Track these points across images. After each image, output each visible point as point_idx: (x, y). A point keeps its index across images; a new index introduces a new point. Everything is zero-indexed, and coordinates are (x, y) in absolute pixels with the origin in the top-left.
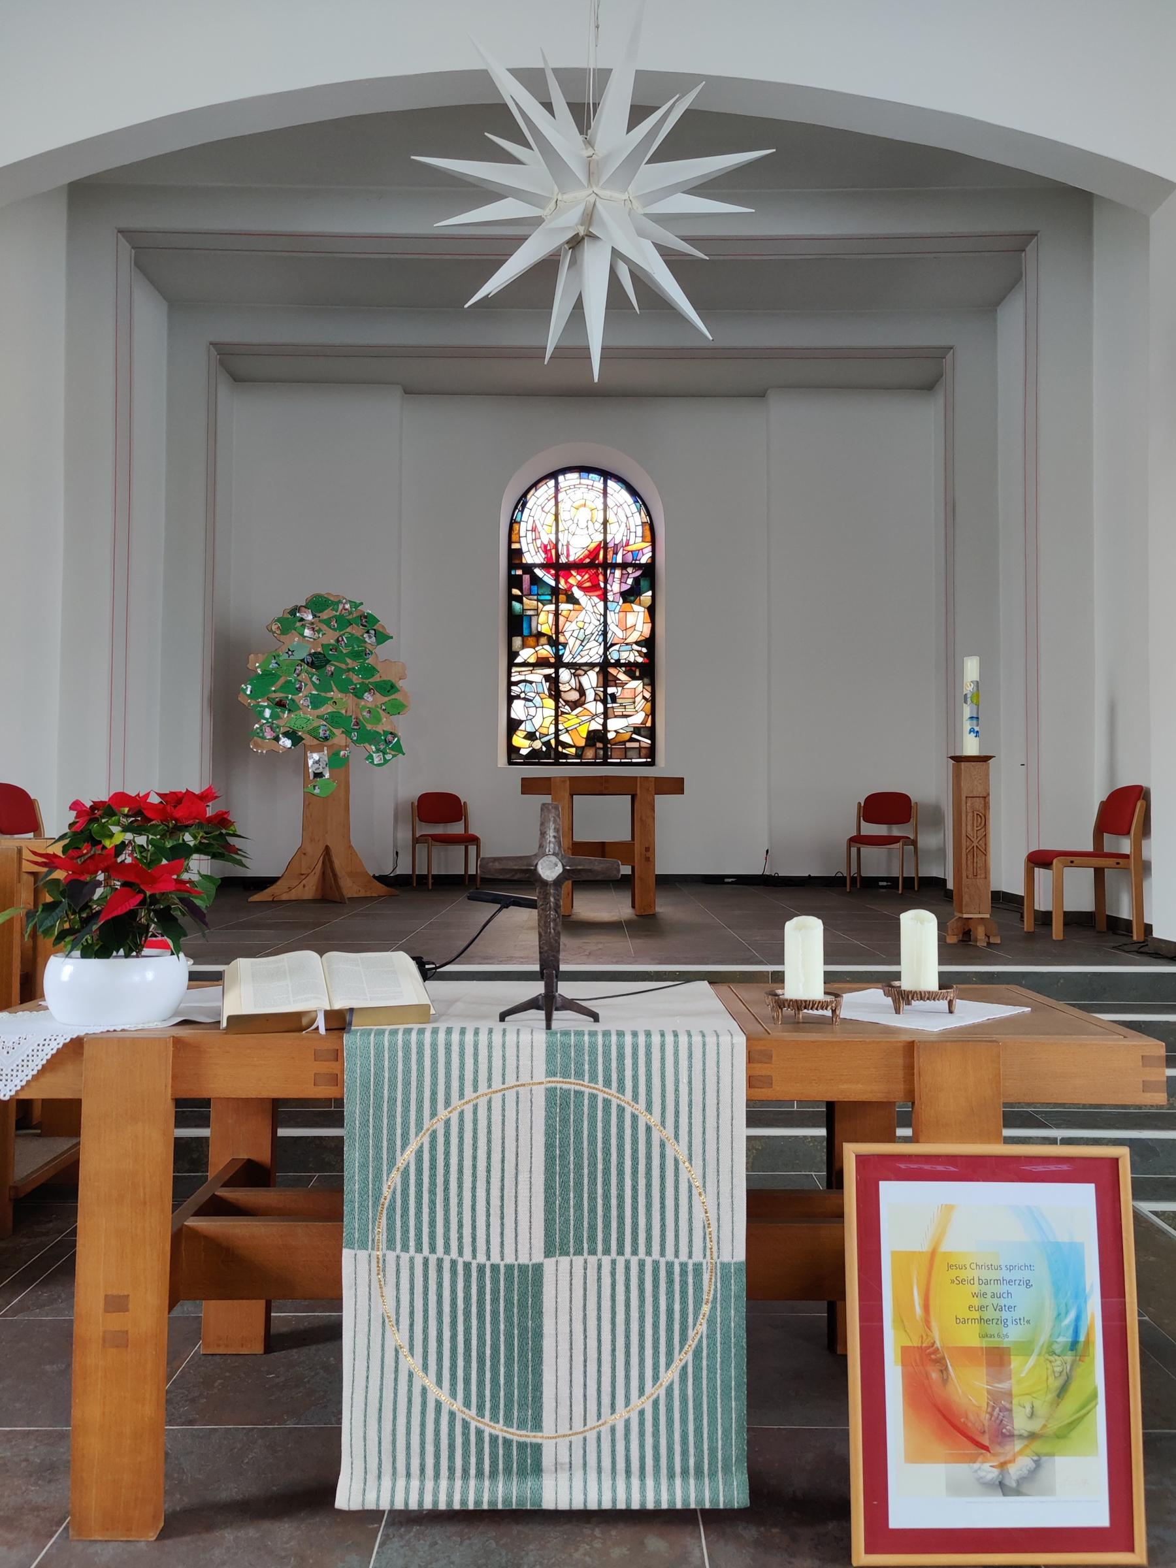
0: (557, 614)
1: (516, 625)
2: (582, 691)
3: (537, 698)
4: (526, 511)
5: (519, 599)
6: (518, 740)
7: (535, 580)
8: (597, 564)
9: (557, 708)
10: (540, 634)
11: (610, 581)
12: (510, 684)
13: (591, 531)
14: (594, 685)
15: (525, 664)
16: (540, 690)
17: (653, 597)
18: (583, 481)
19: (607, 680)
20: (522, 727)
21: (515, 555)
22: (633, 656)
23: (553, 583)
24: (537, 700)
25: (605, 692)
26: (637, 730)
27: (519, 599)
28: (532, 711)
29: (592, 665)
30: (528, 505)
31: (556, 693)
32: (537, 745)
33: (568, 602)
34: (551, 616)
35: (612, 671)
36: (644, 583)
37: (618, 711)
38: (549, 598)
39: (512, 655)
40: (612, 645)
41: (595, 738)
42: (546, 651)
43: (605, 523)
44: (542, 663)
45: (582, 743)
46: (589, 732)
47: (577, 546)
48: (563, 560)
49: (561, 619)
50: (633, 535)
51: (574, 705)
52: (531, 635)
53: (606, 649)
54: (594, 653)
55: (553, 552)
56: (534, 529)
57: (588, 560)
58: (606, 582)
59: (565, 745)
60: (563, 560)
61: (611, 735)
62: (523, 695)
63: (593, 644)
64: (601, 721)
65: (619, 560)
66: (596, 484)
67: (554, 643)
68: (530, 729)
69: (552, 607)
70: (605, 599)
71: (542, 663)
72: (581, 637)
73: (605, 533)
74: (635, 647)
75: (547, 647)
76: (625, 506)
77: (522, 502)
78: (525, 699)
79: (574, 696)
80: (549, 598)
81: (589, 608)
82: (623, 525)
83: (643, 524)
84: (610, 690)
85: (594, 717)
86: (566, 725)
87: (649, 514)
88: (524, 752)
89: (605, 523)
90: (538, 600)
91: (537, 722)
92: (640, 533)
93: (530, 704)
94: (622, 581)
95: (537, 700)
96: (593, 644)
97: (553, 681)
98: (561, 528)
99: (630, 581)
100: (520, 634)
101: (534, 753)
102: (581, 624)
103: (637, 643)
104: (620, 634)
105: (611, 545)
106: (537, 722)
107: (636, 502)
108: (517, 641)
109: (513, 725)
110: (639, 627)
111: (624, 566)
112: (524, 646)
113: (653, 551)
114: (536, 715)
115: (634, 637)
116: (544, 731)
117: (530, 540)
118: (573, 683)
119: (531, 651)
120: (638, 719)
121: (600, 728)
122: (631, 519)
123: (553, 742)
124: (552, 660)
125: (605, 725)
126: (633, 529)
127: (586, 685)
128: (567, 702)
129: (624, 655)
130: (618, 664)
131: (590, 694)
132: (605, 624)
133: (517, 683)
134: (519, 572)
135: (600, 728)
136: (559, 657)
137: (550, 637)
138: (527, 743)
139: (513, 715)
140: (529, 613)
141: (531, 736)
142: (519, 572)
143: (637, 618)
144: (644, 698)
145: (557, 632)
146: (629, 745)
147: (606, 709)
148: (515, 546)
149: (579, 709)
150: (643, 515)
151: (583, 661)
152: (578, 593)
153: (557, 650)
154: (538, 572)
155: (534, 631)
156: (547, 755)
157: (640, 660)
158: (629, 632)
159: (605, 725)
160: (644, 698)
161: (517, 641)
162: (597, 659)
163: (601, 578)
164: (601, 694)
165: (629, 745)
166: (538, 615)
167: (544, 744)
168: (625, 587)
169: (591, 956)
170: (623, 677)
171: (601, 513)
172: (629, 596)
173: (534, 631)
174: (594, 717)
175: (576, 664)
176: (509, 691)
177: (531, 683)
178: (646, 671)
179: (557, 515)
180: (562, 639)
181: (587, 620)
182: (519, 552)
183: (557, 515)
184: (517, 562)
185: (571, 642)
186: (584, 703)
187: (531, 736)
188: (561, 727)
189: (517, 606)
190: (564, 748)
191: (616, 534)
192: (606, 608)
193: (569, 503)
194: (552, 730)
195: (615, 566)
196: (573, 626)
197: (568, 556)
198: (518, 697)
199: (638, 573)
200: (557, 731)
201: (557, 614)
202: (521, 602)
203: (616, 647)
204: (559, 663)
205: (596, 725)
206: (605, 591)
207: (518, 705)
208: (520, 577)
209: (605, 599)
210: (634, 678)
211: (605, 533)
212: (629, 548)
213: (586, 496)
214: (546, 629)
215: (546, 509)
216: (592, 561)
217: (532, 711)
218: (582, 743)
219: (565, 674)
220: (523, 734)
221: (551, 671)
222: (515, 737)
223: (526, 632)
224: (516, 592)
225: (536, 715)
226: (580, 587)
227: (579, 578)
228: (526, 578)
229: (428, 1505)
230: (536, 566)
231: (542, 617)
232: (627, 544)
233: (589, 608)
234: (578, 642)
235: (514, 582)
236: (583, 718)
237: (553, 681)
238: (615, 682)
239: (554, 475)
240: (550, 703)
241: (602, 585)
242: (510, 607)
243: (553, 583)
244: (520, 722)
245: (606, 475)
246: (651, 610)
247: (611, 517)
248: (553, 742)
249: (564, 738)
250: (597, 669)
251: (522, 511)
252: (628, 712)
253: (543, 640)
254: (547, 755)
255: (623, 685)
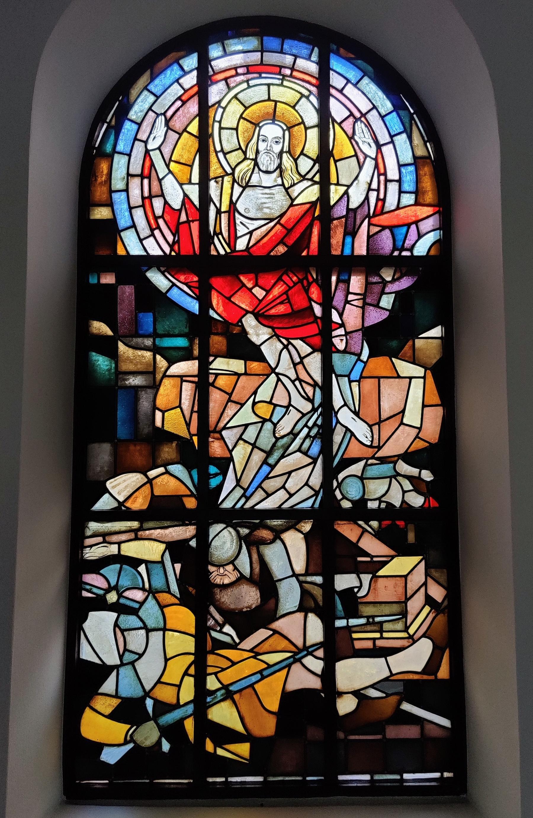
0: (203, 384)
1: (101, 422)
2: (265, 582)
3: (151, 603)
4: (128, 128)
5: (108, 346)
6: (98, 726)
7: (153, 300)
8: (308, 255)
9: (201, 633)
10: (164, 436)
11: (338, 299)
12: (78, 566)
13: (290, 177)
14: (300, 566)
15: (120, 513)
16: (158, 582)
17: (448, 342)
18: (271, 58)
19: (330, 553)
20: (109, 686)
21: (95, 239)
22: (399, 492)
23: (194, 306)
24: (150, 612)
25: (328, 586)
26: (412, 688)
27: (108, 346)
28: (136, 640)
29: (292, 517)
30: (135, 113)
31: (197, 589)
32: (148, 734)
33: (230, 354)
34: (188, 389)
35: (348, 531)
36: (422, 309)
37: (363, 639)
38: (181, 342)
39: (85, 490)
40: (347, 462)
41: (307, 710)
42: (174, 479)
43: (325, 157)
44: (162, 510)
45: (267, 727)
46: (288, 697)
47: (256, 209)
48: (220, 248)
49: (216, 398)
50: (393, 188)
51: (247, 622)
52: (136, 437)
53: (330, 473)
54: (298, 482)
55: (195, 227)
56: (147, 172)
57: (281, 249)
58: (327, 304)
59: (225, 735)
60: (220, 248)
61: (346, 705)
62: (112, 597)
63: (296, 459)
64: (317, 666)
65: (361, 248)
66: (301, 63)
67: (199, 454)
68: (129, 689)
69: (188, 367)
70: (326, 350)
71: (162, 510)
72: (266, 441)
73: (325, 184)
74: (403, 467)
75: (177, 469)
76: (373, 117)
77: (114, 105)
78: (120, 609)
79: (250, 597)
80: (181, 342)
81: (285, 367)
82: (369, 165)
83: (417, 161)
84: (343, 582)
85: (299, 653)
86: (227, 677)
87: (432, 135)
88: (111, 756)
89: (325, 157)
90: (156, 350)
91: (149, 669)
92: (409, 185)
93: (130, 621)
94: (368, 300)
95: (150, 612)
96: (296, 459)
97: (193, 560)
98: (214, 170)
99: (387, 301)
100: (108, 434)
101: (139, 758)
102: (264, 410)
103: (408, 457)
104: (361, 430)
105: (340, 211)
106: (149, 669)
107: (398, 107)
108: (102, 454)
109: (82, 680)
110: (412, 417)
111: (371, 264)
112: (117, 471)
113: (446, 225)
114: (151, 652)
115: (399, 442)
116: (166, 694)
117: (136, 199)
118: (244, 563)
119: (134, 479)
120: (415, 658)
121: (315, 683)
122: (388, 150)
123: (189, 725)
124: (191, 503)
125: (328, 676)
126: (393, 173)
127: (278, 568)
128: (231, 616)
129: (376, 488)
130: (360, 511)
131: (289, 595)
132: (327, 409)
133: (97, 566)
134: (109, 279)
135: (315, 683)
136: (208, 495)
137: (184, 444)
138: (119, 730)
139: (86, 653)
140: (135, 381)
141: (129, 711)
142: (109, 279)
143: (408, 398)
144: (429, 600)
145: (206, 430)
146: (394, 732)
147: (329, 629)
148: (101, 213)
149: (262, 634)
150: (417, 140)
151: (269, 504)
152: (257, 332)
153: (204, 477)
154: (159, 280)
155: (146, 430)
156: (171, 764)
157: (417, 501)
158: (387, 429)
159: (328, 676)
160: (429, 600)
161: (102, 454)
162: (305, 500)
163: (315, 293)
164: (318, 592)
165: (394, 732)
166: (155, 386)
167: (166, 731)
168: (375, 317)
169: (276, 234)
170: (372, 546)
171: (313, 135)
172: (387, 339)
173: (146, 430)
174: (299, 653)
175: (253, 512)
176: (74, 584)
177: (135, 563)
178: (435, 530)
179: (204, 138)
180: (216, 449)
181: (281, 399)
182: (111, 230)
183: (204, 138)
184: (104, 252)
185: (240, 454)
186: (275, 618)
187: (129, 711)
188: (212, 683)
189: (102, 362)
190: (217, 744)
191: (353, 185)
192: (328, 369)
193: (235, 109)
194: (188, 693)
195: (349, 264)
196: (246, 415)
197: (233, 237)
198: (100, 604)
199: (405, 283)
200: (202, 694)
201: (203, 384)
202: (112, 353)
203: (356, 469)
204: (208, 511)
205: (304, 677)
206: (327, 326)
207: (99, 626)
208: (111, 289)
209: (326, 350)
210: (402, 549)
211: (325, 184)
212: (383, 220)
213: (277, 93)
214: (173, 422)
215: (178, 123)
216: (294, 250)
217: (136, 640)
218: (267, 727)
219: (224, 541)
220: (106, 705)
221: (184, 532)
222: (88, 715)
223: (122, 431)
224: (100, 327)
225: (151, 652)
226: (261, 317)
227: (259, 293)
228: (127, 291)
229: (347, 251)
230: (149, 261)
231: (166, 392)
232: (380, 211)
233: (285, 367)
234: (258, 457)
235: (91, 302)
236: (273, 658)
237: (193, 560)
238: (350, 558)
239: (197, 40)
240: (184, 617)
241: (318, 310)
242: (83, 369)
243: (194, 306)
244: (103, 671)
245: (328, 41)
246: (444, 376)
247: (341, 144)
248: (189, 725)
249: (223, 714)
250: (307, 527)
251: (117, 129)
252: (392, 637)
253: (168, 451)
254: (171, 764)
255: (374, 567)
